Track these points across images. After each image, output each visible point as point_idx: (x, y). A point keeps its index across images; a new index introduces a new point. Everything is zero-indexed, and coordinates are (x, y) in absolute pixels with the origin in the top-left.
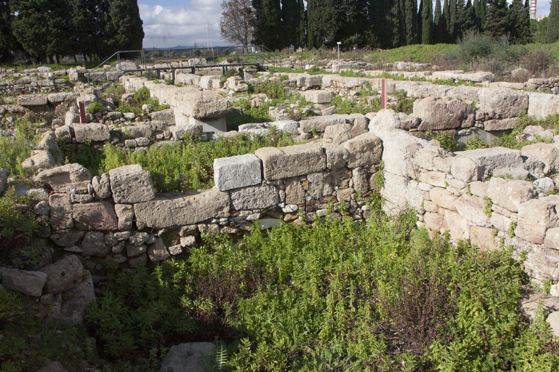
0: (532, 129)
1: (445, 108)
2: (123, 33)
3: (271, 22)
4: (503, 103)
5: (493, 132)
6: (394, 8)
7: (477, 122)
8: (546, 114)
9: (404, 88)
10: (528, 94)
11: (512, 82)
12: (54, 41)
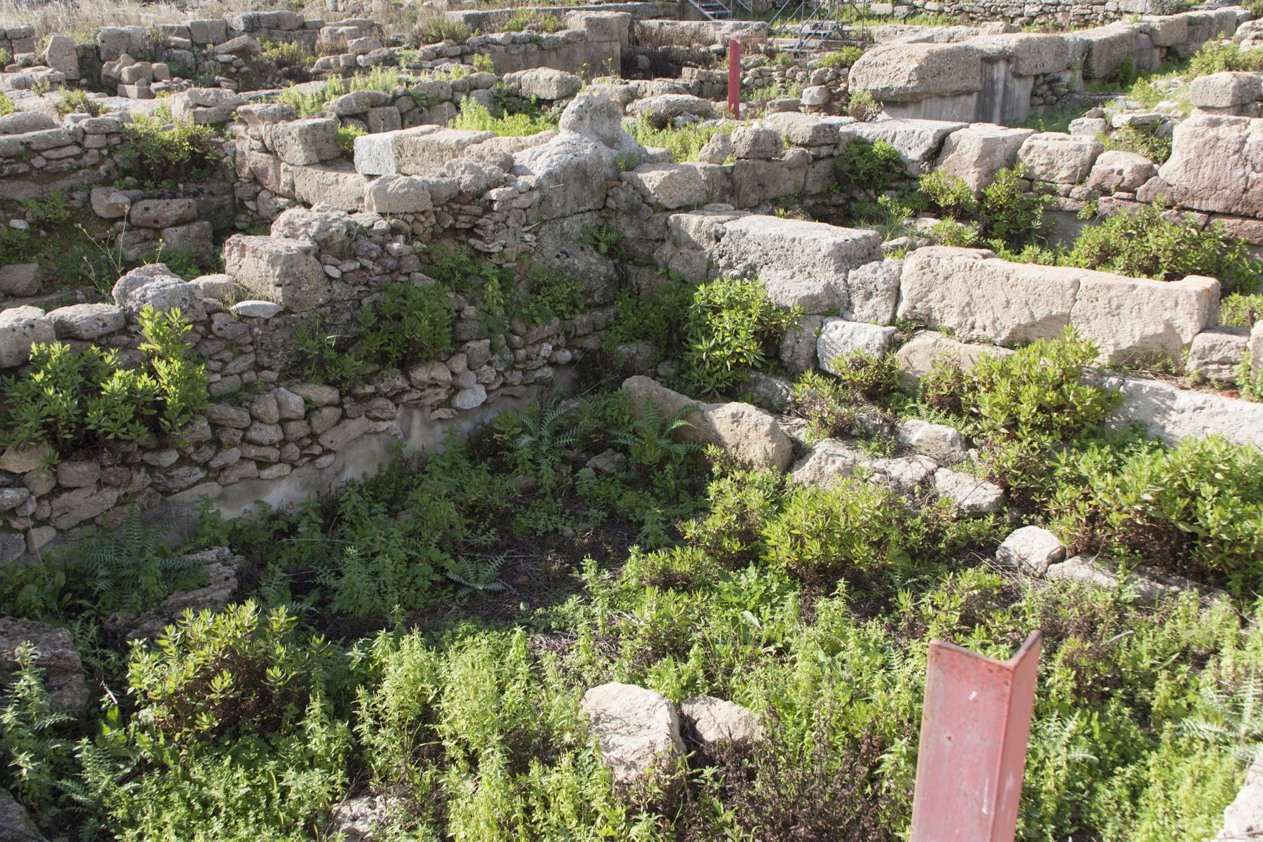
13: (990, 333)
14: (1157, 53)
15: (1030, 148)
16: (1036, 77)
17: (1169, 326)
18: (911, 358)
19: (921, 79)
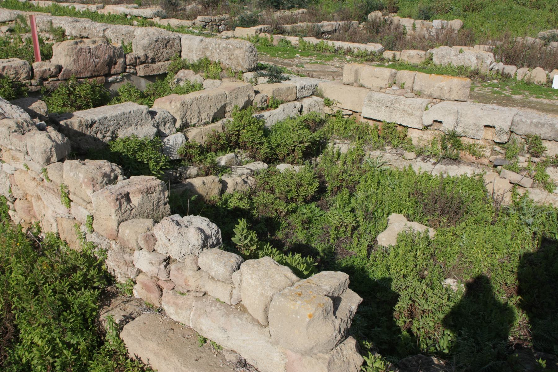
0: (184, 73)
1: (89, 52)
4: (155, 46)
5: (146, 77)
7: (128, 67)
8: (197, 57)
9: (61, 25)
10: (180, 35)
11: (183, 19)
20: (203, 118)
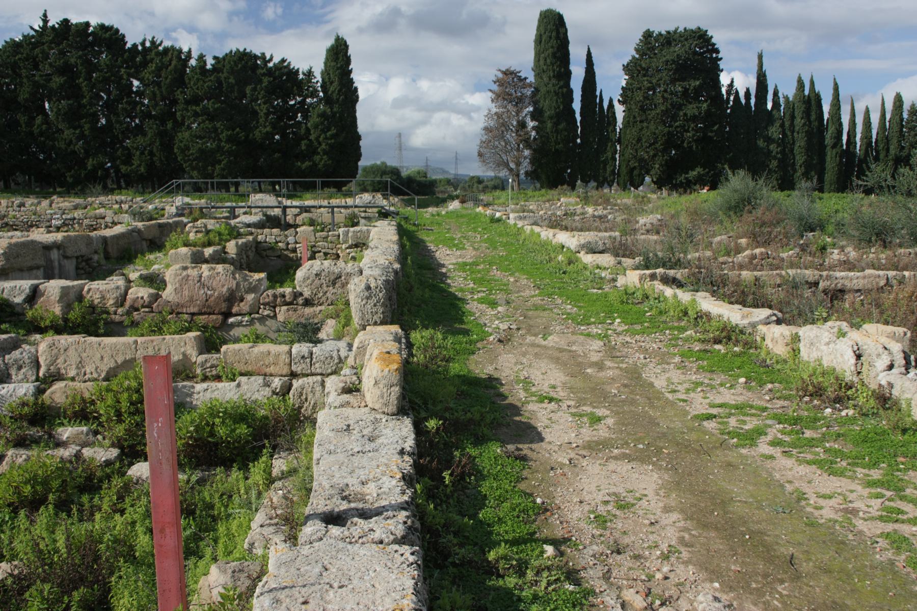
1: (199, 281)
2: (325, 152)
3: (557, 143)
6: (774, 129)
12: (225, 162)
13: (95, 375)
14: (144, 243)
15: (89, 290)
16: (77, 258)
17: (184, 354)
18: (53, 396)
19: (7, 259)
20: (88, 371)
